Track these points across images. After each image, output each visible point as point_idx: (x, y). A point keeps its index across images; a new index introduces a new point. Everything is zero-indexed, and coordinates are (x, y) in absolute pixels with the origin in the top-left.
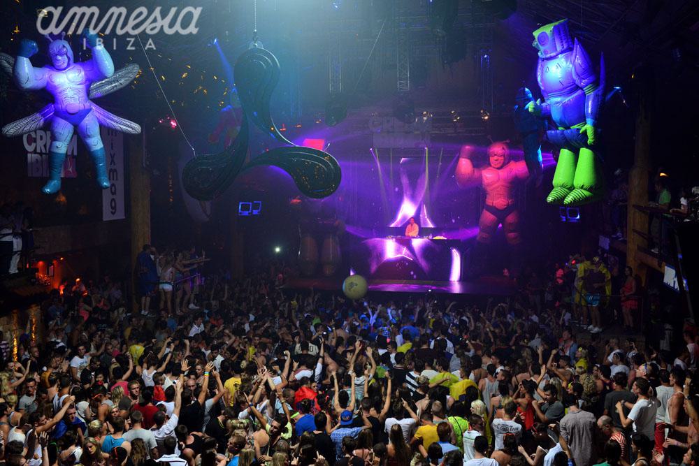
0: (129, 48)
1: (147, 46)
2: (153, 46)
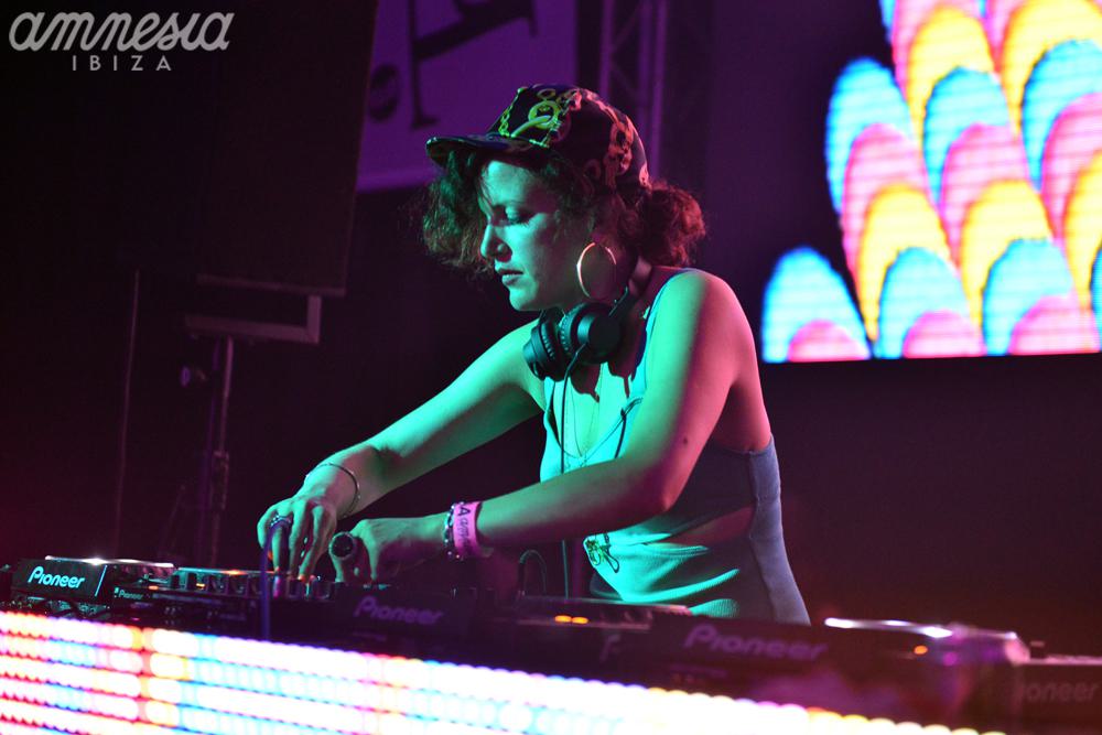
0: (134, 68)
1: (160, 67)
2: (167, 67)
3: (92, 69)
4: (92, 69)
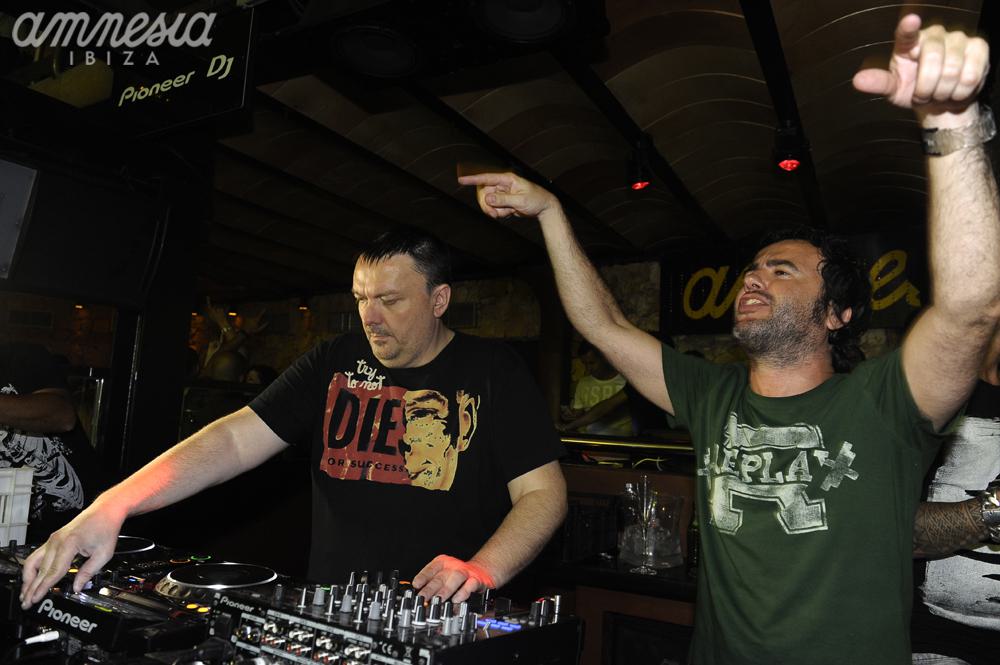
0: (126, 63)
1: (149, 62)
2: (156, 61)
3: (88, 63)
4: (88, 63)
